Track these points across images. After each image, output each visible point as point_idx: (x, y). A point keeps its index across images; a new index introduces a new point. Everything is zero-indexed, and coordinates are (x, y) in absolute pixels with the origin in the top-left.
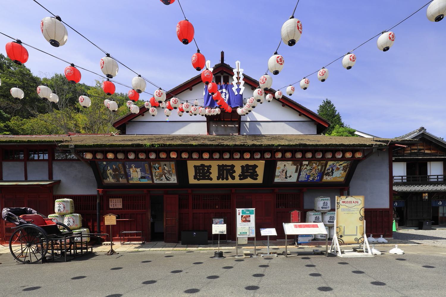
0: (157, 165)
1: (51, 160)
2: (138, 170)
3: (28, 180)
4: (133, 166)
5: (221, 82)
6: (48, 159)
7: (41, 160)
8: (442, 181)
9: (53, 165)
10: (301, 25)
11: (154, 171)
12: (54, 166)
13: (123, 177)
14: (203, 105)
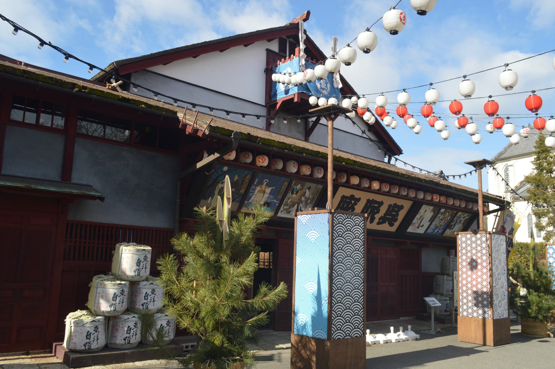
0: (299, 186)
1: (70, 135)
2: (268, 190)
3: (73, 181)
4: (266, 181)
5: (299, 46)
6: (35, 123)
7: (29, 126)
8: (51, 182)
9: (76, 147)
10: (404, 17)
11: (289, 195)
12: (77, 149)
13: (237, 199)
14: (510, 168)
